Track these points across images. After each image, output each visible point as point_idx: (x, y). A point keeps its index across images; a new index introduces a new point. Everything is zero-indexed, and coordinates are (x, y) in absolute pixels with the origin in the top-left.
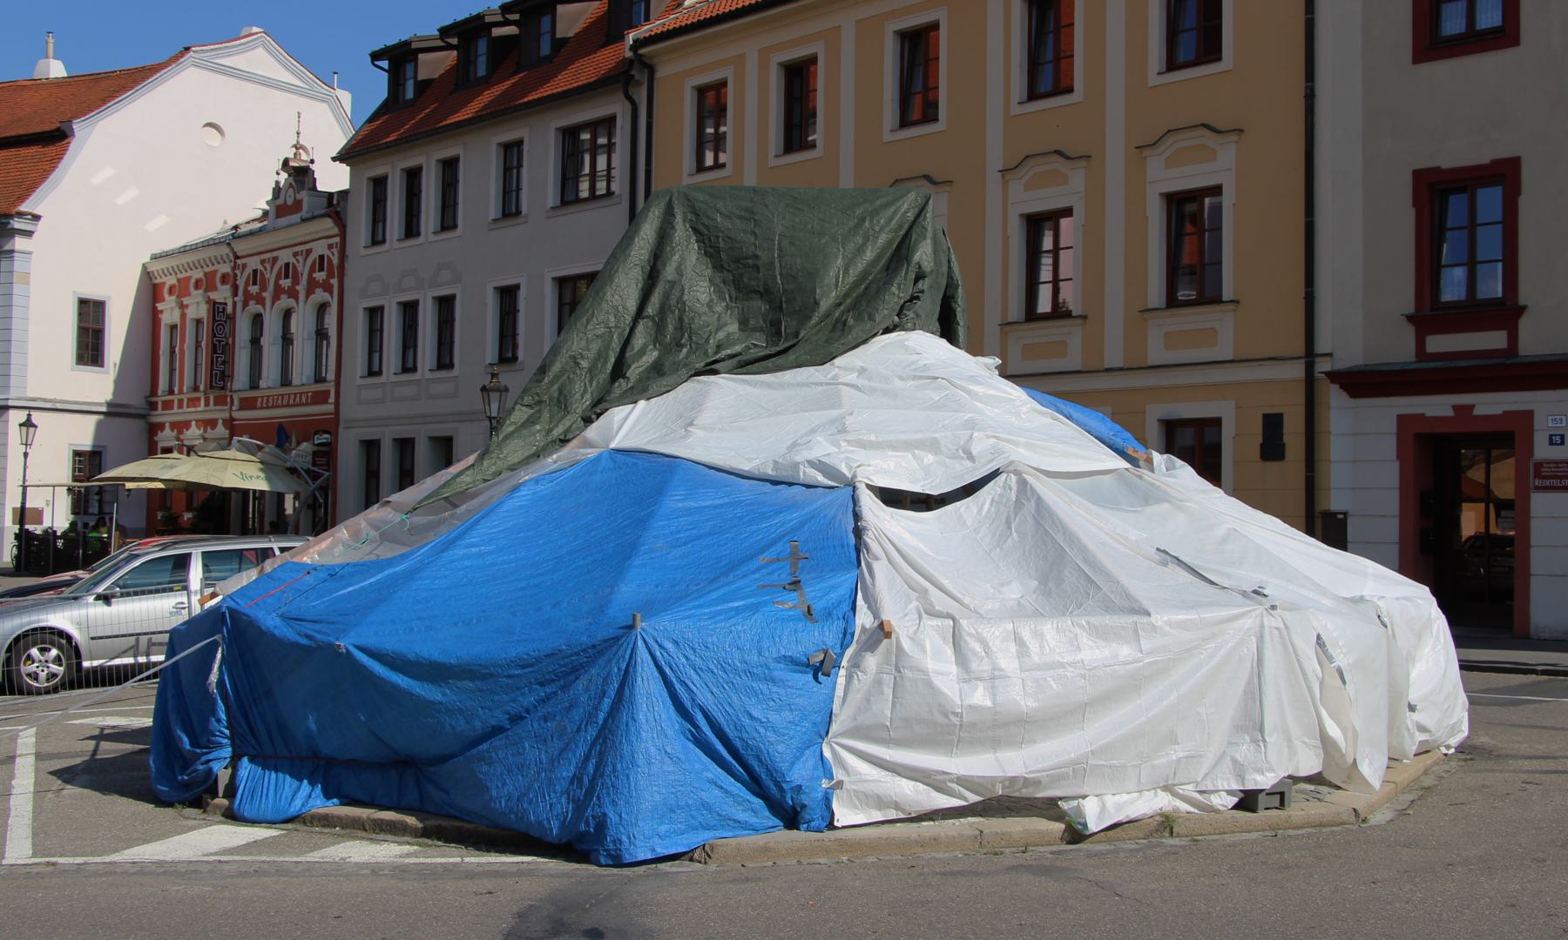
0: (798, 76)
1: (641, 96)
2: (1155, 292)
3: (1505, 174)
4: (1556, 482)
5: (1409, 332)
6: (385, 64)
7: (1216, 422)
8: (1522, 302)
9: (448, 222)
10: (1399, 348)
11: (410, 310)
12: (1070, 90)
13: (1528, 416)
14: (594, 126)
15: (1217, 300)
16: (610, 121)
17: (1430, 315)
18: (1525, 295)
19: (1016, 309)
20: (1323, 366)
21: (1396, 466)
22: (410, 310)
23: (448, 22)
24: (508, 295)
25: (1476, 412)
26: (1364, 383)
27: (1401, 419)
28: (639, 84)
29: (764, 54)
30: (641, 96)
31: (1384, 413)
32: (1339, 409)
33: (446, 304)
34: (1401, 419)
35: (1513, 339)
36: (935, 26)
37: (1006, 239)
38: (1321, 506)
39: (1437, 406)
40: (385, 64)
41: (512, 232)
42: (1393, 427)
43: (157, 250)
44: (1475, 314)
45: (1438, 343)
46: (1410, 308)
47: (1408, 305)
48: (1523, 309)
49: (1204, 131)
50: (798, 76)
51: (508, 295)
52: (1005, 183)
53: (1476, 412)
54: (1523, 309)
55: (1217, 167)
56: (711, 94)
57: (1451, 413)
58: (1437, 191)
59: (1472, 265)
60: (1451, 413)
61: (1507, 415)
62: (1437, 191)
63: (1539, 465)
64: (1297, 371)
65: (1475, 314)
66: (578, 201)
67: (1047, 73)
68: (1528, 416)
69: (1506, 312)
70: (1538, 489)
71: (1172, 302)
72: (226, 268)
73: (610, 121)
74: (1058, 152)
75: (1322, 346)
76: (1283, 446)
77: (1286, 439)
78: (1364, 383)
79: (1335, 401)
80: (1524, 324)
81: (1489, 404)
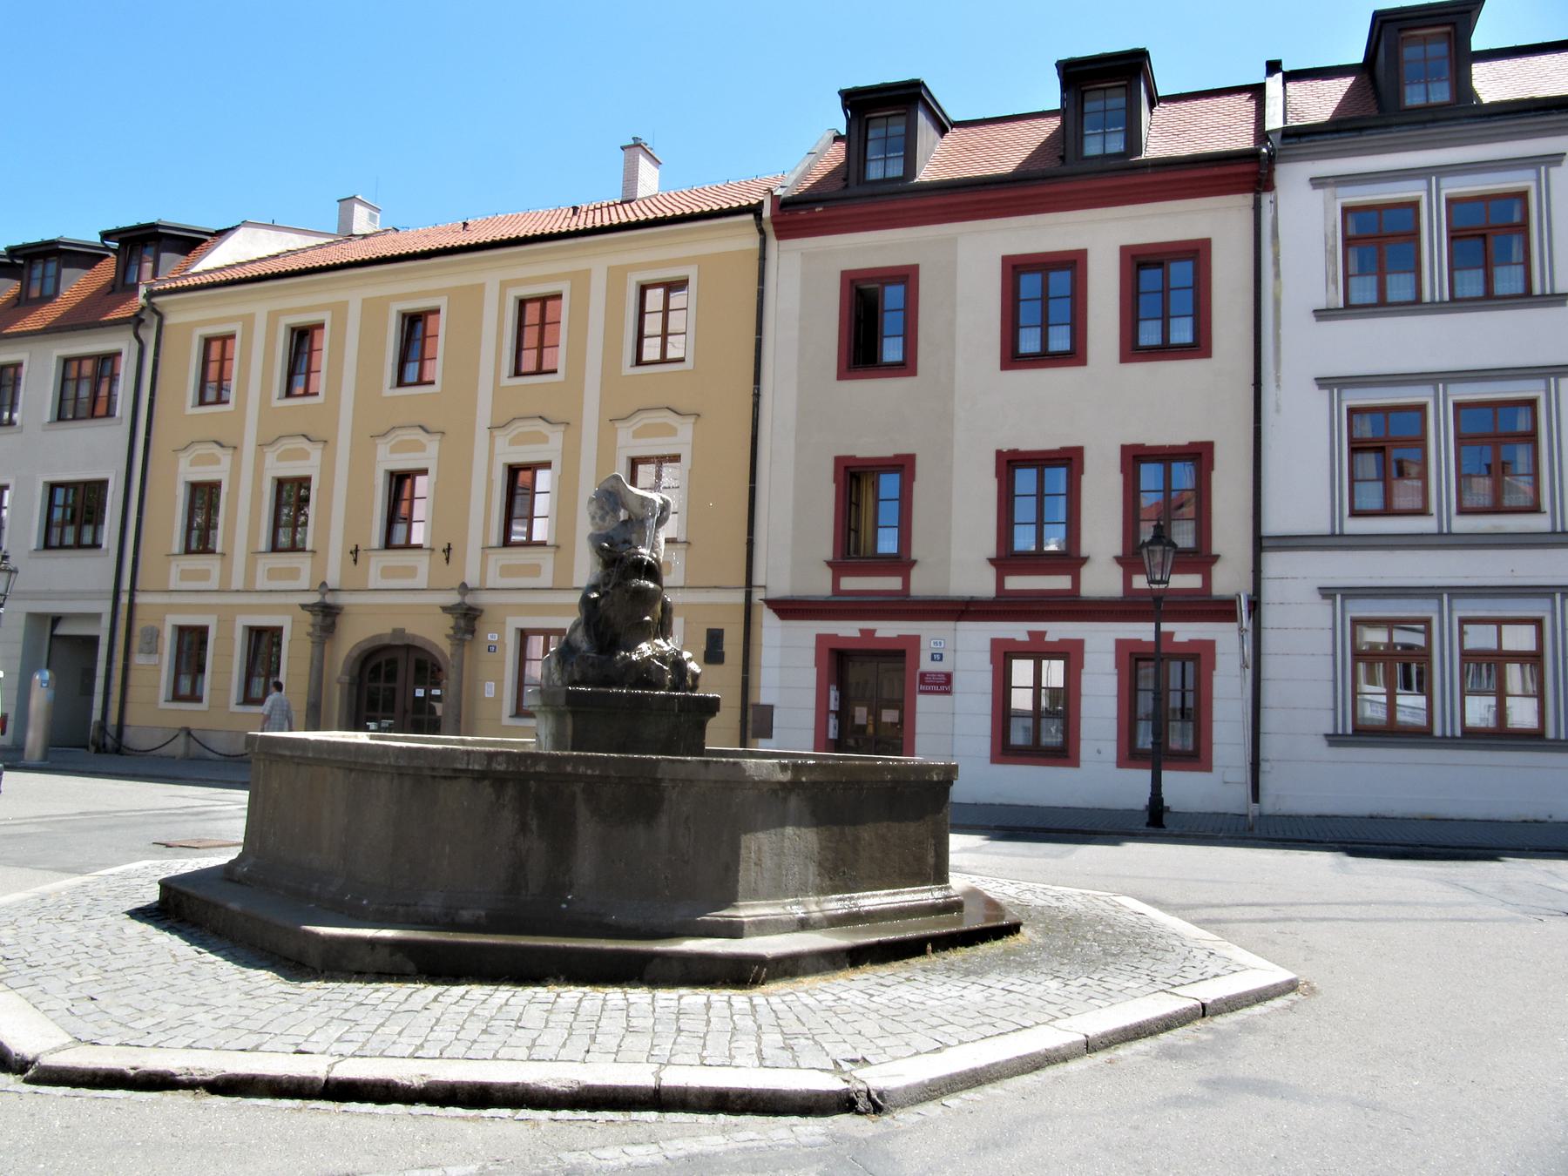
0: (302, 338)
1: (150, 337)
2: (264, 542)
3: (903, 466)
4: (936, 688)
5: (828, 574)
7: (281, 629)
8: (914, 557)
10: (819, 584)
12: (227, 402)
13: (915, 640)
15: (213, 552)
16: (113, 357)
17: (1007, 560)
18: (916, 553)
19: (495, 536)
20: (758, 595)
21: (814, 671)
23: (111, 227)
25: (878, 634)
26: (789, 609)
27: (1120, 644)
28: (148, 327)
29: (504, 285)
30: (150, 337)
31: (808, 632)
32: (770, 627)
34: (1120, 644)
35: (906, 583)
36: (119, 354)
37: (490, 482)
38: (752, 700)
39: (849, 629)
42: (813, 644)
44: (1038, 562)
45: (1015, 583)
46: (1119, 551)
47: (991, 550)
48: (914, 562)
49: (541, 422)
50: (302, 338)
52: (492, 437)
53: (1047, 639)
54: (914, 562)
55: (425, 455)
56: (75, 364)
57: (1025, 638)
58: (854, 478)
59: (1040, 524)
60: (1025, 638)
61: (901, 637)
62: (854, 478)
63: (923, 675)
64: (739, 597)
65: (1038, 562)
67: (299, 381)
68: (915, 640)
69: (901, 563)
70: (922, 692)
71: (275, 548)
74: (422, 427)
75: (759, 579)
76: (722, 654)
77: (725, 648)
78: (789, 609)
79: (768, 622)
80: (915, 574)
81: (888, 629)
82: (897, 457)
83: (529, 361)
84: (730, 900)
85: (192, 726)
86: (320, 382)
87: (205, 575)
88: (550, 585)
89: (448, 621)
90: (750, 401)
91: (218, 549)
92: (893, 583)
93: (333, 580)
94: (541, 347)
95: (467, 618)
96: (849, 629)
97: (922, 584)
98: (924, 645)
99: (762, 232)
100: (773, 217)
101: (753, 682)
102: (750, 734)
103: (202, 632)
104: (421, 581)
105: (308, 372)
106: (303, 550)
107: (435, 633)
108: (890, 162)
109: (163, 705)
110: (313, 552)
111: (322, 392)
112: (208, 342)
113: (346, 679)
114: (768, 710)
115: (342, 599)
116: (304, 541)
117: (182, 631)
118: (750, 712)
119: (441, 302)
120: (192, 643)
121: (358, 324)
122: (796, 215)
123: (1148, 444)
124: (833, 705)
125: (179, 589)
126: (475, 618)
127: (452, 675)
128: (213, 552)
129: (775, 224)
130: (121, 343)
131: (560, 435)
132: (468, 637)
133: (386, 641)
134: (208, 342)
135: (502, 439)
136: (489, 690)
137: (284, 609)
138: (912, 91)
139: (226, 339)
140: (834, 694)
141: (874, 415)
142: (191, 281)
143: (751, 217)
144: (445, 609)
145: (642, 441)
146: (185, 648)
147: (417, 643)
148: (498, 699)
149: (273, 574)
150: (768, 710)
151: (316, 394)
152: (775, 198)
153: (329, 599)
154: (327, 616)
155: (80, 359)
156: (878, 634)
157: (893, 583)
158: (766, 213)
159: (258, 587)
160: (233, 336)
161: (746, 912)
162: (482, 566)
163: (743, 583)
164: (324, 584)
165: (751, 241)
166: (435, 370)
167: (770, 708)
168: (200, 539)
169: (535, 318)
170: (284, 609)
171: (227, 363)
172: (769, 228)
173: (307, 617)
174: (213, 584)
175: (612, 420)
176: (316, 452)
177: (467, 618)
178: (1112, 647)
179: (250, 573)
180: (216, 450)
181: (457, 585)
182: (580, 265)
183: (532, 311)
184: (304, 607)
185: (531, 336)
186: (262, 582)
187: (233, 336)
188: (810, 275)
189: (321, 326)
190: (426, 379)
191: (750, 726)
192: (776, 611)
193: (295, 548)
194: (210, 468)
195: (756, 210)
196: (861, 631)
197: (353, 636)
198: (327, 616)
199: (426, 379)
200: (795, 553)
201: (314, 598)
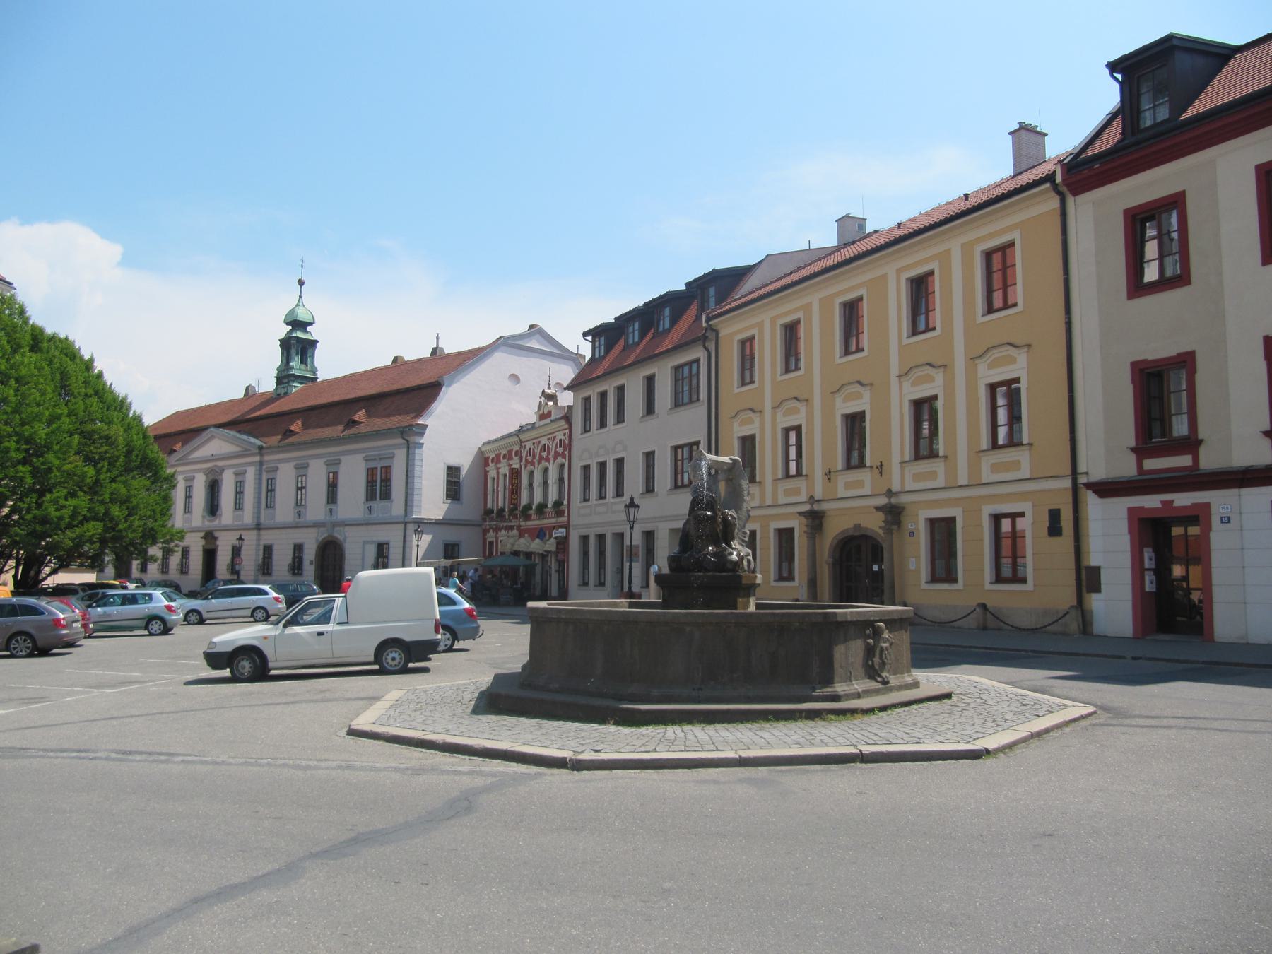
0: (851, 310)
1: (712, 347)
3: (1186, 361)
5: (1132, 458)
6: (590, 338)
8: (1200, 437)
9: (620, 418)
10: (1127, 468)
11: (603, 465)
12: (934, 329)
14: (690, 363)
16: (698, 361)
18: (1202, 434)
20: (1082, 480)
22: (603, 465)
24: (649, 456)
25: (1176, 504)
26: (1106, 489)
27: (1131, 511)
29: (899, 271)
30: (712, 347)
31: (1120, 506)
33: (620, 462)
34: (1131, 511)
38: (1085, 563)
39: (1152, 502)
40: (590, 338)
41: (652, 422)
43: (486, 440)
45: (1151, 464)
46: (1132, 443)
48: (1201, 442)
49: (1009, 347)
50: (851, 310)
51: (649, 456)
52: (900, 383)
54: (1201, 442)
61: (1195, 506)
64: (1067, 483)
66: (683, 404)
69: (1191, 444)
72: (516, 448)
73: (698, 361)
75: (1082, 468)
77: (1063, 524)
78: (1106, 489)
79: (1090, 499)
80: (1203, 451)
81: (1183, 500)
82: (1180, 355)
83: (998, 302)
84: (829, 681)
85: (989, 605)
86: (937, 318)
87: (933, 475)
88: (943, 485)
89: (881, 516)
90: (1063, 327)
91: (1025, 440)
92: (1184, 461)
93: (818, 496)
94: (1005, 288)
95: (894, 514)
96: (1152, 502)
97: (1209, 460)
98: (1214, 510)
99: (1060, 193)
100: (1063, 180)
101: (1084, 548)
102: (1084, 589)
103: (951, 521)
104: (867, 490)
105: (927, 312)
106: (1020, 444)
107: (874, 523)
108: (1158, 109)
109: (988, 586)
110: (1030, 444)
111: (866, 349)
112: (988, 255)
113: (831, 560)
114: (1097, 570)
115: (825, 506)
116: (1021, 438)
117: (932, 522)
118: (1084, 573)
119: (863, 292)
120: (943, 531)
121: (817, 314)
122: (1085, 171)
123: (1150, 358)
124: (1148, 562)
125: (926, 491)
126: (900, 513)
127: (886, 555)
128: (937, 456)
129: (1068, 185)
130: (698, 353)
131: (941, 375)
132: (895, 527)
133: (851, 533)
134: (988, 255)
135: (906, 385)
136: (912, 565)
137: (1023, 496)
138: (1166, 45)
139: (752, 339)
140: (1148, 554)
141: (1159, 327)
142: (736, 303)
143: (1048, 185)
144: (878, 509)
145: (848, 404)
146: (937, 537)
147: (869, 533)
148: (918, 571)
149: (995, 468)
150: (1097, 570)
151: (1015, 305)
152: (1063, 166)
153: (816, 507)
154: (815, 519)
155: (682, 366)
156: (1176, 504)
157: (1184, 461)
158: (1059, 179)
159: (780, 502)
160: (1011, 244)
161: (840, 688)
162: (905, 477)
163: (1069, 472)
164: (812, 497)
165: (1054, 203)
166: (865, 341)
167: (1098, 569)
168: (924, 446)
169: (998, 263)
170: (1023, 496)
171: (1009, 270)
172: (1064, 189)
173: (803, 520)
174: (940, 482)
175: (973, 359)
176: (939, 377)
177: (894, 514)
178: (1125, 515)
179: (974, 467)
180: (930, 370)
181: (884, 491)
182: (805, 301)
183: (997, 258)
184: (800, 514)
185: (997, 277)
186: (782, 499)
187: (1011, 244)
188: (1098, 216)
189: (931, 273)
190: (931, 326)
191: (1084, 583)
192: (1095, 492)
193: (933, 455)
194: (925, 386)
195: (1050, 178)
196: (1162, 502)
197: (835, 528)
198: (815, 519)
199: (931, 326)
200: (1107, 445)
201: (806, 508)
